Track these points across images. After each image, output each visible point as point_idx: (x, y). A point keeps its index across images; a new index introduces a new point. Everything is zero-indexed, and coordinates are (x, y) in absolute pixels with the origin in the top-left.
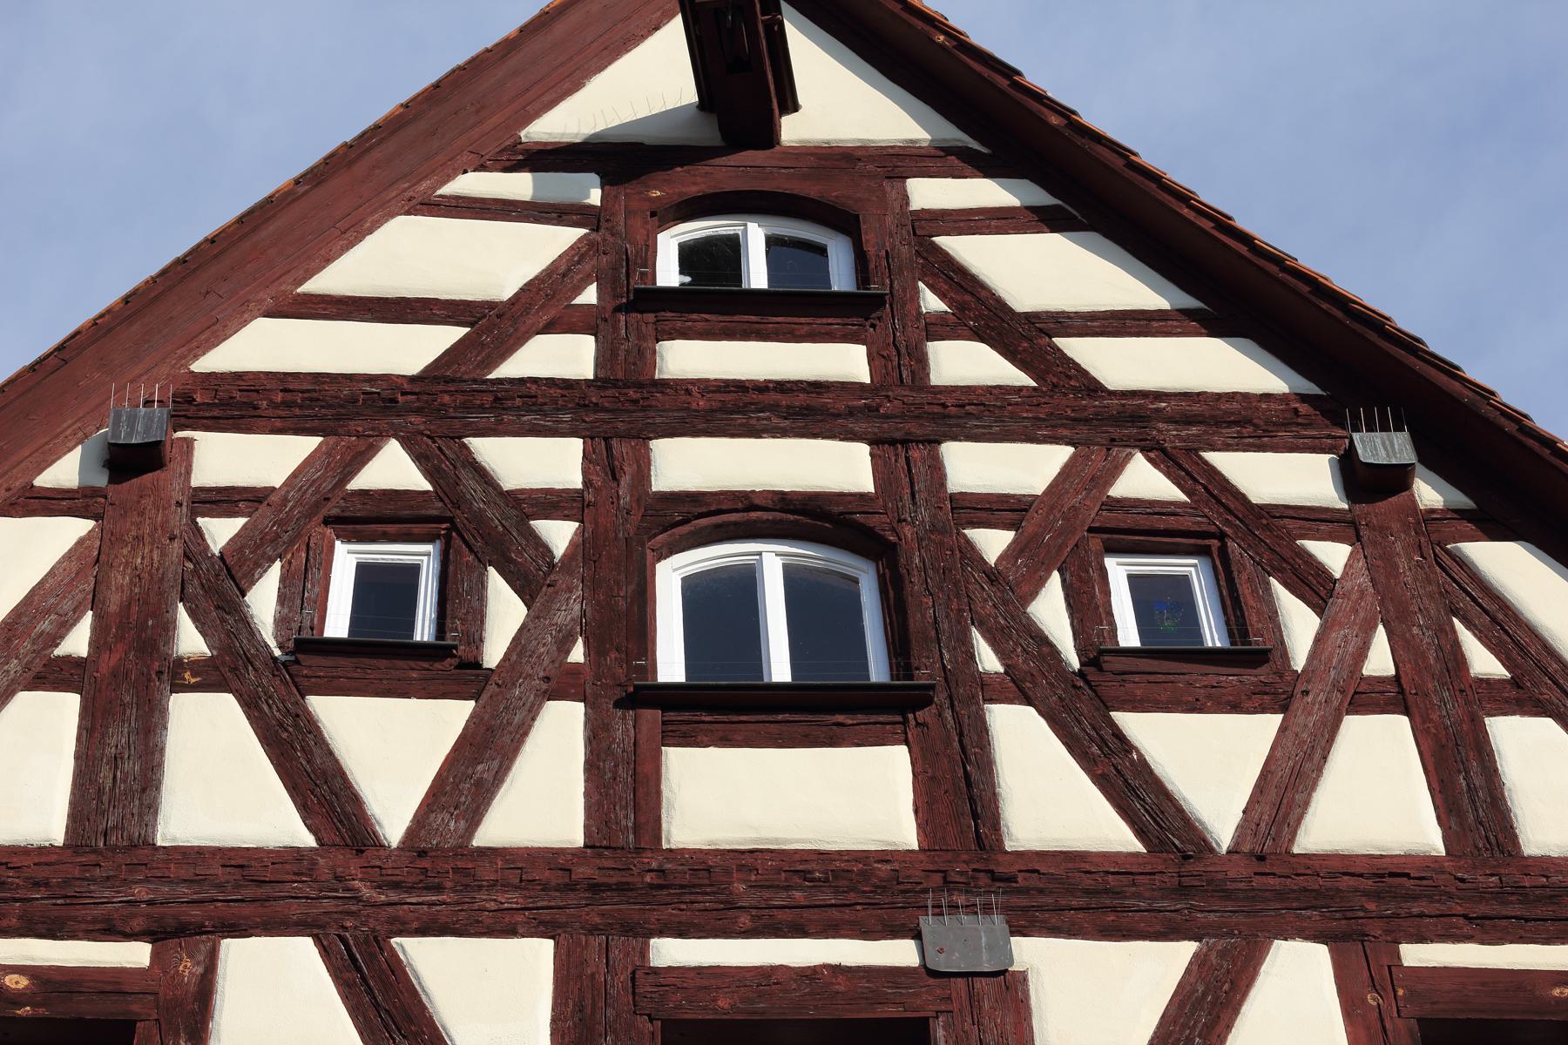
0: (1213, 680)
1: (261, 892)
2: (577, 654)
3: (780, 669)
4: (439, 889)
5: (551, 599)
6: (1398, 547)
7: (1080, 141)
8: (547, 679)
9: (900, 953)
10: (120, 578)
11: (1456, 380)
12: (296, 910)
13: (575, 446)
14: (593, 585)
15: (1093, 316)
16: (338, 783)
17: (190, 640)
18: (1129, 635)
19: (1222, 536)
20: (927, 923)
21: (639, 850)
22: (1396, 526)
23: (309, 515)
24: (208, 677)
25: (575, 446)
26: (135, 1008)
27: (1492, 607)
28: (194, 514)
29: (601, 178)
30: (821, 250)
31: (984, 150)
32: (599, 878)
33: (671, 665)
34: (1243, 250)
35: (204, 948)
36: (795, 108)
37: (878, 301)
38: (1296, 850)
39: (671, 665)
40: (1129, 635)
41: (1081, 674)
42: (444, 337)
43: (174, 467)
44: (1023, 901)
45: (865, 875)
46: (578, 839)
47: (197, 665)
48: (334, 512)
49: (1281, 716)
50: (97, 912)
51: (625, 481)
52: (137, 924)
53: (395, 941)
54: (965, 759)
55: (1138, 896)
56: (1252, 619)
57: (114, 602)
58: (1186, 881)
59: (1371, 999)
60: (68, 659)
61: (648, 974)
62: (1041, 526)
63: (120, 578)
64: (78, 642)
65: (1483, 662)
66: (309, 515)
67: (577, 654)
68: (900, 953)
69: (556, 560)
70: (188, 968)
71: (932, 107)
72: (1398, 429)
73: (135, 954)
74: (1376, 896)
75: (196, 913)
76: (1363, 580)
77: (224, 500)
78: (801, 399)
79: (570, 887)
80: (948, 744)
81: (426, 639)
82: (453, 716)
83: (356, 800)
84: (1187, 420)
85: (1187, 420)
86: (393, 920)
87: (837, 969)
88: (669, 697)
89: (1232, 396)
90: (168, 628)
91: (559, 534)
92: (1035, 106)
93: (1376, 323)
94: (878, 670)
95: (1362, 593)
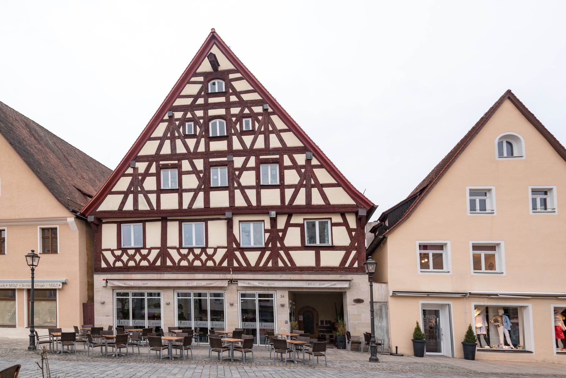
2: (204, 134)
9: (225, 159)
11: (383, 239)
13: (202, 111)
20: (228, 156)
25: (202, 111)
28: (175, 121)
29: (190, 105)
30: (222, 83)
36: (220, 66)
47: (177, 137)
51: (206, 115)
52: (177, 160)
57: (171, 131)
59: (257, 161)
60: (168, 137)
62: (273, 349)
64: (169, 135)
67: (204, 134)
68: (225, 159)
70: (180, 163)
73: (176, 162)
81: (132, 325)
82: (195, 140)
87: (222, 161)
90: (175, 134)
91: (201, 121)
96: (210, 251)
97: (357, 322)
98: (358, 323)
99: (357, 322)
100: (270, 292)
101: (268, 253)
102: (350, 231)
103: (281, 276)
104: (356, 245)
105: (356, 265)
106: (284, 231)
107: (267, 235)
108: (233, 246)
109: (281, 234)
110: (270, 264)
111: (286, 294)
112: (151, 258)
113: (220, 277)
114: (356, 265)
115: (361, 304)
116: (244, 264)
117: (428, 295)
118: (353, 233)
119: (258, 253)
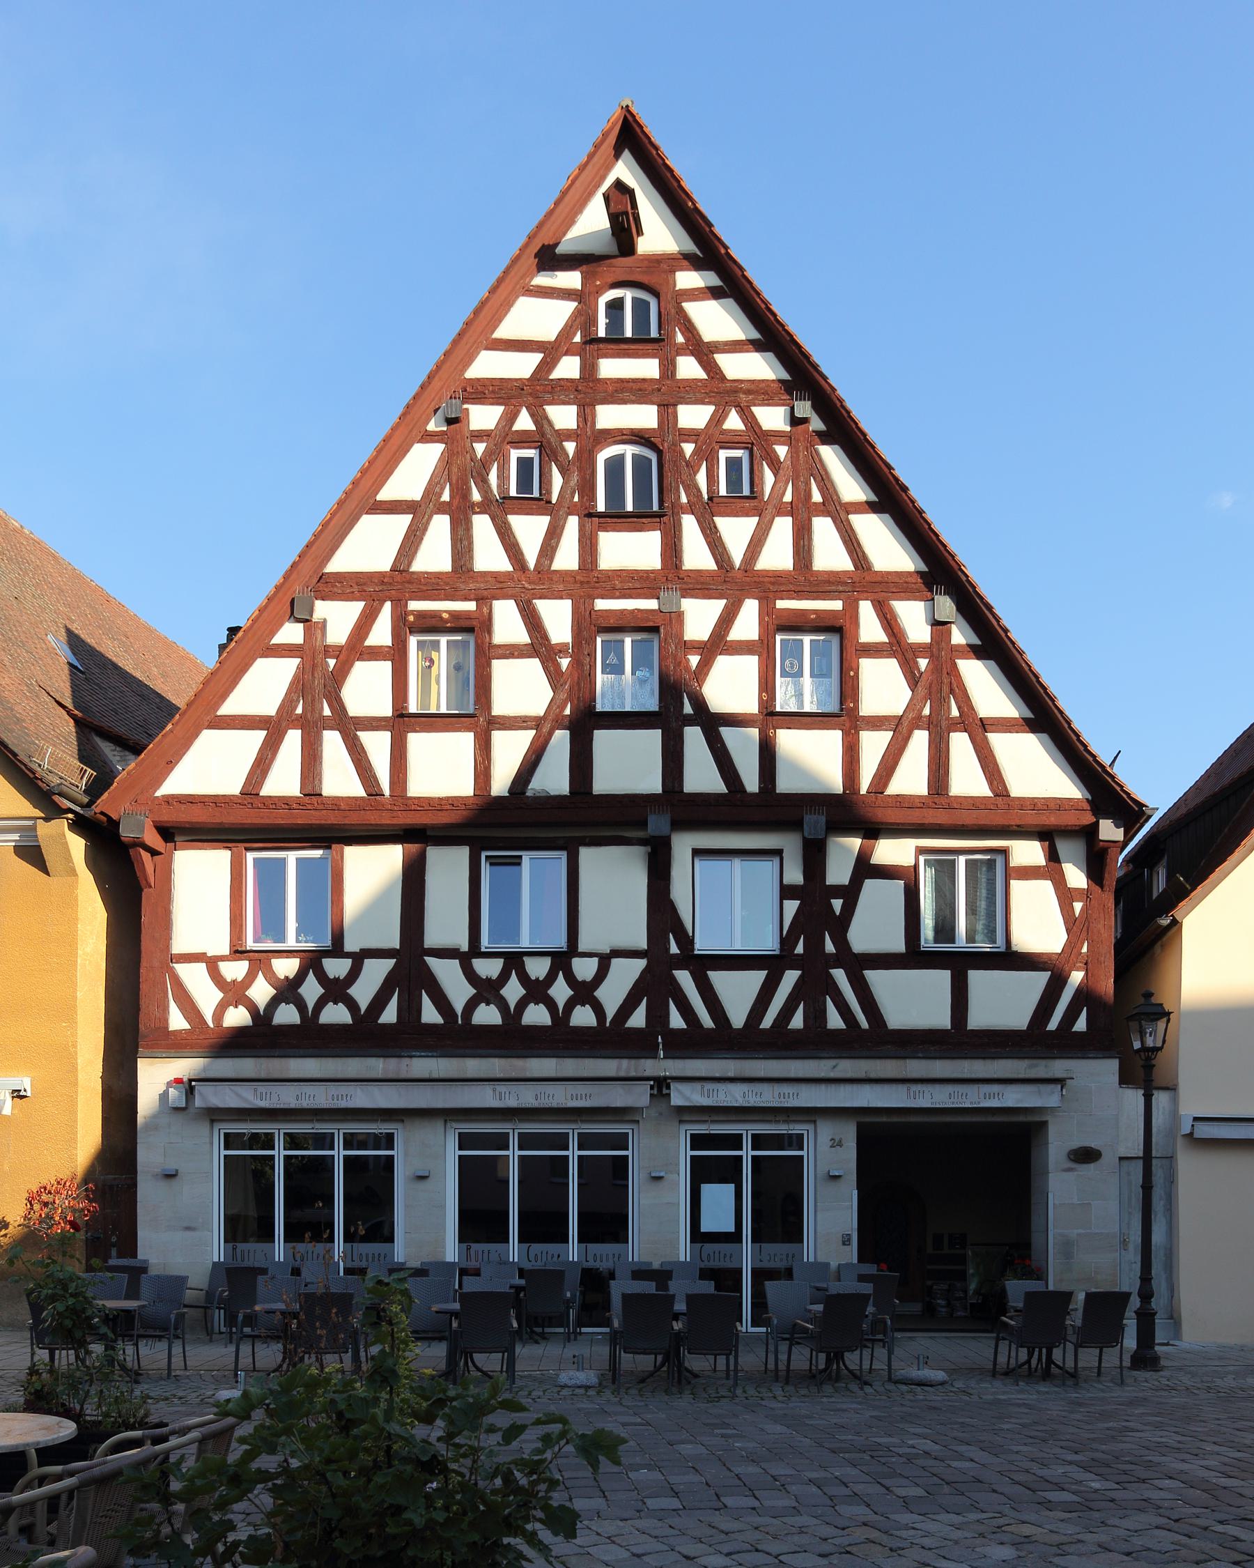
0: (742, 505)
1: (501, 586)
3: (629, 507)
4: (543, 584)
5: (569, 476)
6: (801, 448)
7: (730, 263)
8: (569, 508)
9: (652, 604)
10: (455, 470)
12: (510, 592)
14: (580, 470)
15: (726, 343)
16: (517, 548)
17: (476, 496)
18: (723, 491)
19: (753, 444)
21: (592, 570)
22: (802, 439)
23: (502, 442)
24: (561, 650)
26: (475, 623)
27: (823, 473)
31: (701, 256)
32: (582, 580)
33: (601, 507)
34: (772, 319)
35: (489, 604)
37: (663, 340)
38: (755, 569)
39: (601, 507)
40: (723, 491)
41: (707, 503)
42: (535, 359)
43: (464, 422)
44: (685, 586)
45: (648, 577)
46: (576, 567)
48: (510, 440)
49: (757, 519)
50: (462, 593)
53: (534, 601)
54: (675, 537)
55: (714, 584)
56: (756, 479)
58: (727, 579)
61: (17, 1282)
63: (455, 470)
64: (446, 497)
65: (817, 497)
66: (502, 442)
68: (652, 604)
69: (527, 1487)
70: (485, 610)
71: (687, 232)
72: (808, 400)
73: (471, 606)
74: (773, 584)
75: (485, 593)
76: (789, 462)
77: (480, 435)
78: (639, 386)
79: (575, 582)
80: (670, 531)
83: (522, 554)
84: (748, 392)
85: (748, 392)
86: (533, 594)
88: (600, 515)
89: (763, 381)
92: (717, 243)
93: (807, 357)
94: (655, 508)
95: (788, 468)
96: (585, 969)
97: (1076, 1231)
98: (1079, 1235)
99: (1076, 1231)
100: (796, 1129)
101: (790, 978)
102: (1065, 895)
103: (834, 1067)
104: (1085, 950)
105: (1081, 1025)
106: (851, 893)
107: (792, 906)
108: (668, 949)
109: (837, 904)
110: (797, 1021)
111: (849, 1133)
112: (363, 992)
113: (619, 1069)
114: (1081, 1025)
115: (1092, 1166)
116: (707, 1021)
117: (313, 1129)
118: (1078, 906)
119: (758, 977)
